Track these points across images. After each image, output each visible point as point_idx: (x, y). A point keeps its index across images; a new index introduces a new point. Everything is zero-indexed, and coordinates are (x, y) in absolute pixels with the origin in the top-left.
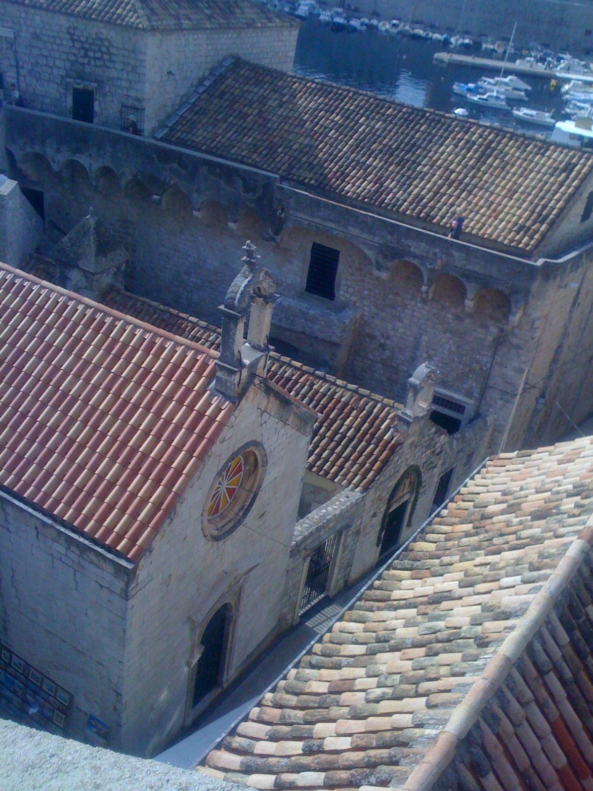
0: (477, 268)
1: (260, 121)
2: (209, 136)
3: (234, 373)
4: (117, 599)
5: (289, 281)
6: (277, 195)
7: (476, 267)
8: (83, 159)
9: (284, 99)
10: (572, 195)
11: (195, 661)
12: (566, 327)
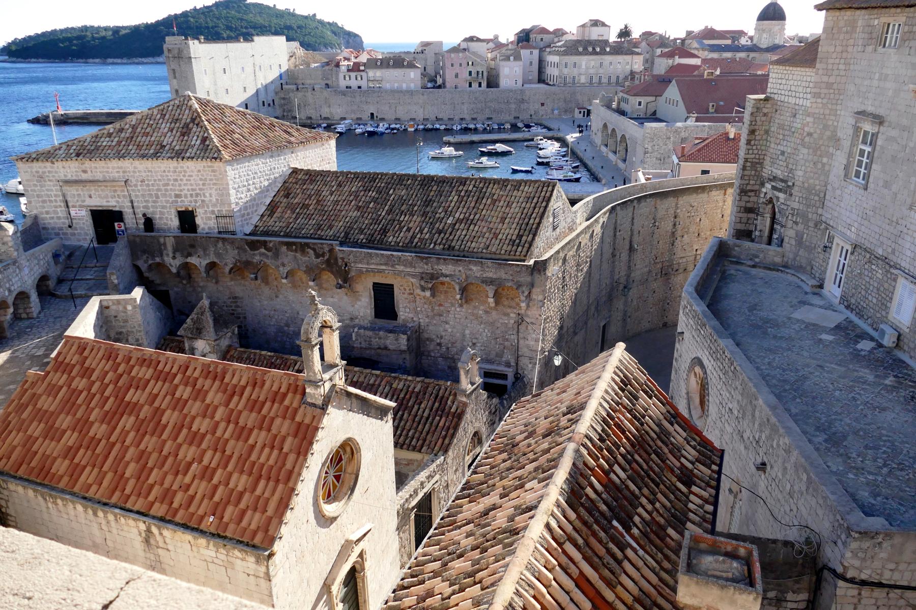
0: (490, 275)
1: (319, 207)
2: (284, 225)
4: (263, 583)
5: (362, 314)
8: (193, 260)
9: (333, 189)
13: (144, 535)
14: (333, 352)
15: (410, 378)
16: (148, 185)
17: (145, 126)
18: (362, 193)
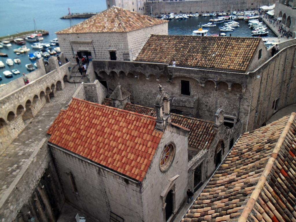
0: (230, 78)
1: (161, 50)
2: (148, 57)
3: (161, 123)
4: (138, 193)
6: (169, 69)
7: (230, 78)
8: (115, 70)
10: (254, 52)
11: (164, 208)
12: (260, 90)
13: (98, 171)
14: (167, 109)
15: (195, 119)
16: (99, 42)
17: (99, 19)
18: (178, 44)
